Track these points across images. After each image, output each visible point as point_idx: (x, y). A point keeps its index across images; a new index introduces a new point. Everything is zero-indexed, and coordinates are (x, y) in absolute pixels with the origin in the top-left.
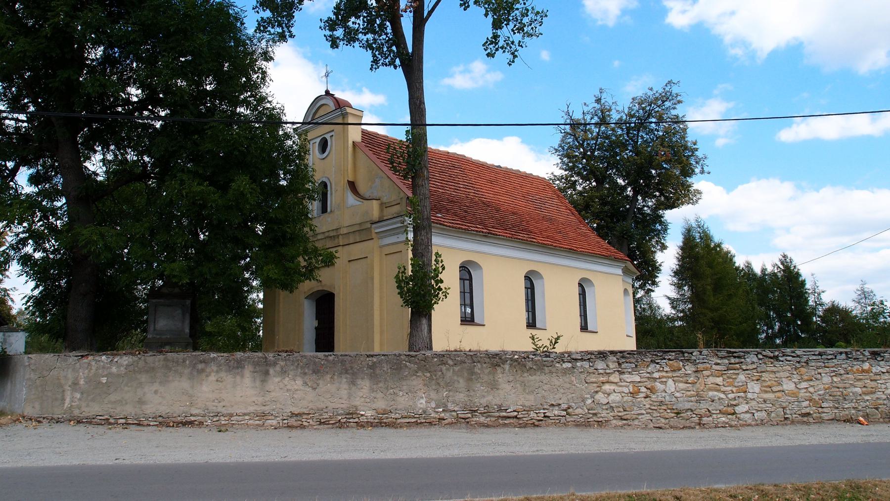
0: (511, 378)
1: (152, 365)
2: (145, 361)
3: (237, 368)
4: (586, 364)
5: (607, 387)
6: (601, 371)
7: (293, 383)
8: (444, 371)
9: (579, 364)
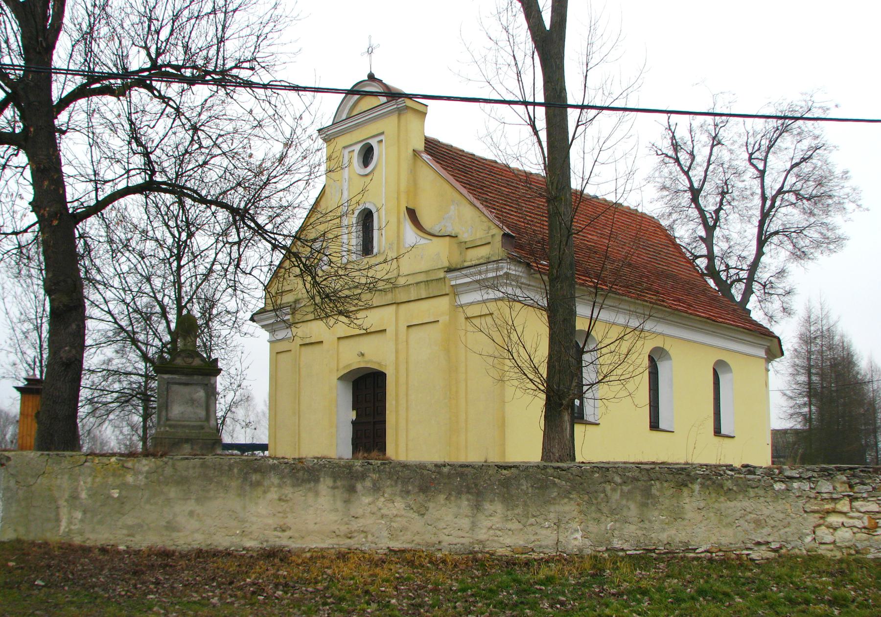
0: (702, 504)
1: (185, 474)
2: (173, 466)
3: (309, 481)
4: (806, 486)
5: (834, 519)
6: (825, 496)
7: (391, 505)
8: (609, 492)
9: (796, 485)
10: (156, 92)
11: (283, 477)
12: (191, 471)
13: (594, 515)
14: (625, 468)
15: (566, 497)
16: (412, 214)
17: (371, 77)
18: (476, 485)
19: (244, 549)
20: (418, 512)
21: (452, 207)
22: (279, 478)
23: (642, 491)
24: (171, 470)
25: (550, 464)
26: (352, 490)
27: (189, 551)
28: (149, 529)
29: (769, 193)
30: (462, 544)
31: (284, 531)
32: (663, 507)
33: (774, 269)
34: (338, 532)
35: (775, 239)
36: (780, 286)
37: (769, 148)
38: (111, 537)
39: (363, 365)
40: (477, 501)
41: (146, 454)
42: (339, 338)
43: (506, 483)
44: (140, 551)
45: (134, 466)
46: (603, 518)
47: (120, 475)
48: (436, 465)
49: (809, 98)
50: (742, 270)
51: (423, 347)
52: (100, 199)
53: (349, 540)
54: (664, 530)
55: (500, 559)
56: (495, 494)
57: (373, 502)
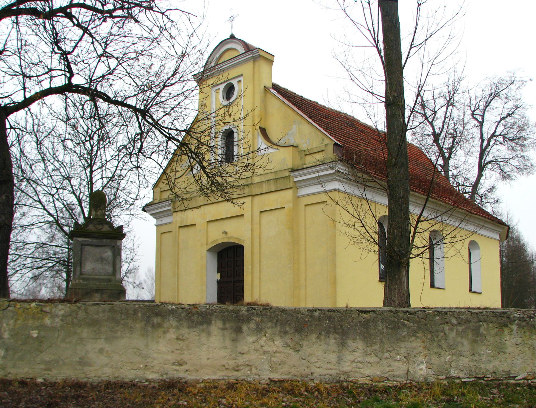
0: (519, 341)
1: (96, 317)
2: (86, 310)
3: (202, 323)
7: (271, 343)
8: (447, 331)
10: (74, 20)
11: (181, 320)
12: (101, 315)
13: (436, 350)
14: (460, 312)
15: (413, 335)
16: (263, 131)
17: (232, 37)
18: (341, 326)
19: (147, 381)
20: (294, 349)
21: (294, 126)
22: (177, 321)
23: (472, 330)
24: (84, 313)
25: (400, 309)
26: (238, 330)
27: (99, 383)
28: (64, 364)
29: (486, 136)
30: (330, 375)
31: (181, 365)
32: (489, 343)
33: (487, 186)
34: (227, 367)
35: (489, 166)
36: (492, 197)
37: (486, 107)
38: (31, 371)
39: (226, 240)
40: (342, 339)
41: (62, 301)
42: (208, 222)
43: (365, 325)
44: (56, 383)
45: (51, 310)
46: (443, 353)
47: (39, 318)
48: (309, 310)
49: (512, 75)
50: (467, 186)
51: (273, 227)
52: (27, 96)
53: (236, 373)
54: (490, 361)
55: (362, 386)
56: (357, 333)
57: (257, 341)
